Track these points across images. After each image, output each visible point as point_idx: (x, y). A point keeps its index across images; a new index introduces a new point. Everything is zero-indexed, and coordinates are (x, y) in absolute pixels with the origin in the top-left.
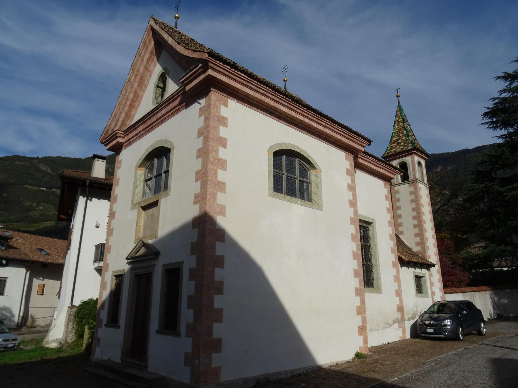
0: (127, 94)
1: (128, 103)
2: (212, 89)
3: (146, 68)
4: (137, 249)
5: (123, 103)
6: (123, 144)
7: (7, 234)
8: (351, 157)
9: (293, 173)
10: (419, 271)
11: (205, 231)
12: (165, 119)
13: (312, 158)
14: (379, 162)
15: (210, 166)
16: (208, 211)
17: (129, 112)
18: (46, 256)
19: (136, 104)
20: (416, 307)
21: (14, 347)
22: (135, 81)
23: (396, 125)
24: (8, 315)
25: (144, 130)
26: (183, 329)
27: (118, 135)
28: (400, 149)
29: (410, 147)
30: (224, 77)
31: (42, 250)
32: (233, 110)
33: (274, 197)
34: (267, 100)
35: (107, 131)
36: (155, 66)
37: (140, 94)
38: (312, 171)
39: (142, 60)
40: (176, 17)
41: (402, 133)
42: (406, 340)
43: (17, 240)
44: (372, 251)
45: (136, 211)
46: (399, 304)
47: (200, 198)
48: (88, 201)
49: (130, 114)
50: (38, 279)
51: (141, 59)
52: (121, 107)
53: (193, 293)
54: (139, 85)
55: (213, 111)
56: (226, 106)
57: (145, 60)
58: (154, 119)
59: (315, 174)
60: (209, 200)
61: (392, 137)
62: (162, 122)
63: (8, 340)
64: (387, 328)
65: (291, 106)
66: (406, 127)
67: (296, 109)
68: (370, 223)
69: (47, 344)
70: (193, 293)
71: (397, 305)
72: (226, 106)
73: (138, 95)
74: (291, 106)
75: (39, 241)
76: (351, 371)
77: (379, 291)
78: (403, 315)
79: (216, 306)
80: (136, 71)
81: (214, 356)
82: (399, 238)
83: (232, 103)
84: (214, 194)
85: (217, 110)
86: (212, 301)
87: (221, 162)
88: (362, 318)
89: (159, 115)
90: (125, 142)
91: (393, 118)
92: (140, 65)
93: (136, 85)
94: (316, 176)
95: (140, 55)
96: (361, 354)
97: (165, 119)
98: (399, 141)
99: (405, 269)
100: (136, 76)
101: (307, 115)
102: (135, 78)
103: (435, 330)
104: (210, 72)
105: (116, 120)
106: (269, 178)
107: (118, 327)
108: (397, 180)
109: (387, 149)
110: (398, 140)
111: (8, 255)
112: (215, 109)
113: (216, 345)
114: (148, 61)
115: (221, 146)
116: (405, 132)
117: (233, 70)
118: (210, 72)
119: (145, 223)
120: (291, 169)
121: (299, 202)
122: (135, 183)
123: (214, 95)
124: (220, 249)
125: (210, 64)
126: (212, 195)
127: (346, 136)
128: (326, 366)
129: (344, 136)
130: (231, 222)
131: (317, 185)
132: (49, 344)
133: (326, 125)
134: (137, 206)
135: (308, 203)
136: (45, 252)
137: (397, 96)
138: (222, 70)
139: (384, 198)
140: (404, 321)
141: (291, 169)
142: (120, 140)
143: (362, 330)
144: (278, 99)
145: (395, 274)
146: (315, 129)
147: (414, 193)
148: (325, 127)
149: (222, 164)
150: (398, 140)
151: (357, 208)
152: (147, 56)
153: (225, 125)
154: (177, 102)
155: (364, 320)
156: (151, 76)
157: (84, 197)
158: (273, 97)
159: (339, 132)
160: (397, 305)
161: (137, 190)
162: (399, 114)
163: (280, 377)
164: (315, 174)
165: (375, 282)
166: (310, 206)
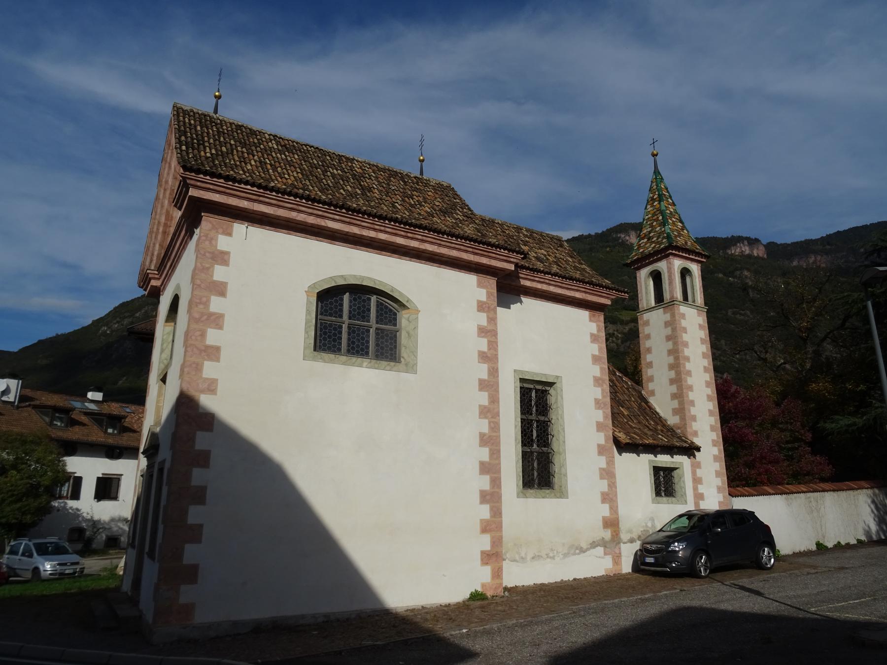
0: (158, 217)
1: (161, 229)
5: (155, 230)
7: (128, 410)
10: (664, 460)
20: (652, 520)
21: (75, 573)
22: (164, 197)
27: (150, 276)
28: (650, 248)
29: (665, 243)
30: (218, 195)
32: (243, 242)
33: (314, 359)
38: (404, 312)
40: (216, 97)
41: (657, 220)
44: (554, 429)
51: (167, 165)
60: (188, 373)
63: (65, 564)
64: (575, 554)
65: (348, 220)
66: (663, 208)
67: (358, 223)
68: (551, 384)
71: (604, 518)
74: (348, 220)
76: (418, 619)
77: (563, 494)
80: (163, 183)
81: (183, 588)
82: (647, 402)
83: (239, 228)
84: (197, 364)
85: (210, 243)
91: (646, 195)
92: (168, 174)
98: (652, 234)
99: (629, 457)
100: (165, 190)
101: (383, 228)
102: (164, 193)
103: (656, 558)
105: (150, 254)
106: (306, 332)
108: (648, 301)
111: (120, 442)
112: (207, 243)
115: (216, 295)
116: (661, 218)
120: (359, 312)
121: (365, 364)
123: (208, 222)
124: (202, 440)
125: (188, 181)
126: (194, 366)
129: (466, 251)
131: (408, 333)
133: (424, 238)
137: (654, 155)
138: (211, 187)
140: (619, 543)
141: (359, 312)
142: (154, 283)
143: (492, 557)
144: (320, 213)
147: (671, 325)
155: (497, 542)
158: (310, 211)
159: (453, 245)
160: (604, 518)
164: (406, 316)
166: (388, 368)
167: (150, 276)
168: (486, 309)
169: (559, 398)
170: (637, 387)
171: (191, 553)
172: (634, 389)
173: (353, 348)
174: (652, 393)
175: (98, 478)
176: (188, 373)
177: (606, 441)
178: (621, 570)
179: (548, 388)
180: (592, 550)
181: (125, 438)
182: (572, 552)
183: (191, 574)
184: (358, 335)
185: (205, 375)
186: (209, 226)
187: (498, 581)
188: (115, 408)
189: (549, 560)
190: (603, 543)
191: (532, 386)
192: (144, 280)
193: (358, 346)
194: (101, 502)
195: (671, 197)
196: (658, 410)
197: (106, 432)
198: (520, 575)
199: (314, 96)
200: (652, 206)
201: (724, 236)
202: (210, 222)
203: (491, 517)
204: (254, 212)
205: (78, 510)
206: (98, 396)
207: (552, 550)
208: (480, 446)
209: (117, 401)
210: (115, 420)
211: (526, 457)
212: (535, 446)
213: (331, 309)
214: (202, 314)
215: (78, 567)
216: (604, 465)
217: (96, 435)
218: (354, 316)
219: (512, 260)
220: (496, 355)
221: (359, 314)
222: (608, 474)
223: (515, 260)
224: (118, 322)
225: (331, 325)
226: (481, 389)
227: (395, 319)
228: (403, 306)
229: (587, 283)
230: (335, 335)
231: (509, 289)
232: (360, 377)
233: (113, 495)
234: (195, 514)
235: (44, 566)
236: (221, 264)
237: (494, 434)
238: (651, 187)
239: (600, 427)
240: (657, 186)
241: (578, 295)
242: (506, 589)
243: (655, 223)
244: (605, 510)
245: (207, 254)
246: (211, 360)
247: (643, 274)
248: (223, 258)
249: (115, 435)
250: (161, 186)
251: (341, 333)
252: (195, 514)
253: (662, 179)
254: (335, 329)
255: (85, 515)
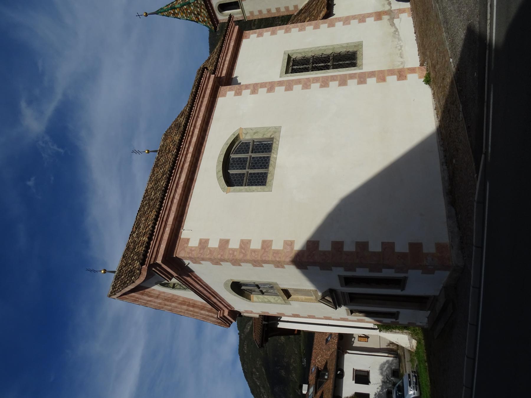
0: (183, 311)
1: (191, 309)
2: (174, 256)
3: (157, 297)
4: (327, 303)
5: (192, 313)
6: (230, 310)
7: (313, 369)
8: (222, 89)
9: (245, 160)
11: (308, 259)
12: (204, 285)
13: (228, 140)
14: (223, 49)
15: (248, 257)
16: (290, 259)
17: (199, 308)
18: (332, 337)
19: (191, 302)
21: (415, 376)
22: (170, 306)
23: (179, 17)
24: (387, 366)
25: (215, 298)
26: (402, 275)
27: (221, 316)
28: (204, 12)
30: (162, 246)
31: (327, 340)
32: (192, 232)
33: (271, 185)
34: (177, 197)
35: (219, 323)
36: (154, 290)
37: (182, 299)
38: (241, 138)
39: (150, 301)
40: (105, 273)
41: (186, 9)
42: (412, 9)
43: (318, 361)
44: (318, 53)
45: (291, 302)
46: (373, 19)
47: (279, 264)
48: (281, 319)
49: (201, 306)
50: (353, 342)
52: (195, 314)
53: (368, 269)
54: (174, 302)
55: (195, 254)
56: (188, 240)
57: (149, 299)
58: (205, 292)
59: (244, 135)
60: (280, 258)
61: (192, 21)
62: (207, 286)
63: (410, 382)
64: (399, 35)
65: (180, 170)
66: (179, 6)
67: (182, 163)
68: (289, 57)
69: (413, 348)
70: (368, 269)
71: (375, 20)
72: (188, 240)
73: (183, 301)
74: (180, 170)
75: (319, 342)
76: (443, 102)
77: (360, 45)
78: (386, 13)
79: (379, 249)
80: (161, 306)
81: (425, 251)
82: (302, 10)
83: (184, 234)
84: (274, 253)
85: (193, 250)
86: (374, 254)
87: (243, 246)
88: (388, 75)
89: (201, 289)
90: (228, 309)
91: (171, 19)
92: (155, 302)
93: (173, 304)
94: (246, 134)
95: (146, 303)
96: (426, 77)
97: (204, 285)
98: (196, 13)
99: (335, 10)
100: (165, 305)
101: (186, 149)
102: (168, 305)
104: (159, 261)
105: (207, 317)
106: (253, 191)
107: (398, 313)
108: (238, 13)
109: (205, 26)
110: (195, 14)
111: (333, 370)
112: (193, 253)
113: (416, 247)
114: (151, 296)
115: (228, 245)
116: (185, 7)
117: (153, 237)
118: (159, 261)
119: (302, 295)
120: (241, 164)
121: (275, 156)
122: (265, 302)
123: (180, 253)
124: (325, 246)
126: (275, 255)
127: (201, 99)
128: (438, 123)
129: (202, 102)
130: (299, 235)
131: (255, 133)
132: (413, 346)
133: (193, 125)
134: (287, 301)
135: (274, 140)
136: (328, 337)
137: (147, 15)
138: (156, 249)
139: (260, 38)
140: (391, 11)
141: (241, 164)
142: (226, 314)
143: (401, 74)
144: (175, 185)
145: (342, 23)
146: (198, 138)
148: (195, 126)
149: (245, 244)
150: (195, 14)
151: (274, 82)
152: (146, 297)
153: (207, 241)
154: (189, 279)
155: (391, 72)
156: (164, 293)
157: (278, 324)
158: (173, 191)
159: (198, 109)
160: (375, 20)
161: (272, 300)
162: (166, 13)
163: (447, 178)
164: (244, 135)
165: (351, 50)
166: (277, 143)
167: (221, 316)
168: (240, 91)
169: (298, 51)
170: (292, 18)
171: (401, 247)
172: (293, 20)
173: (265, 166)
174: (296, 7)
175: (356, 383)
176: (280, 258)
177: (326, 23)
178: (408, 8)
179: (292, 59)
180: (396, 25)
181: (331, 368)
182: (397, 36)
183: (416, 247)
184: (256, 163)
185: (281, 248)
186: (183, 252)
187: (417, 70)
188: (312, 377)
189: (403, 49)
190: (391, 20)
191: (291, 68)
192: (225, 322)
193: (263, 163)
194: (371, 381)
195: (172, 3)
196: (306, 2)
197: (327, 379)
198: (412, 56)
199: (112, 234)
200: (178, 14)
201: (208, 33)
202: (180, 251)
203: (375, 77)
204: (174, 224)
205: (375, 395)
206: (305, 387)
207: (396, 47)
208: (328, 87)
209: (308, 376)
210: (320, 374)
211: (335, 67)
212: (329, 64)
213: (239, 180)
214: (241, 252)
215: (411, 374)
216: (341, 23)
217: (329, 385)
218: (243, 167)
219: (208, 76)
220: (269, 83)
221: (242, 164)
222: (347, 20)
223: (208, 74)
224: (263, 395)
225: (249, 180)
226: (292, 89)
227: (246, 143)
228: (237, 138)
229: (224, 38)
230: (256, 177)
231: (229, 80)
232: (282, 159)
233: (366, 374)
234: (375, 247)
235: (411, 395)
236: (208, 244)
237: (321, 80)
238: (167, 16)
239: (316, 27)
240: (165, 11)
241: (232, 44)
242: (422, 65)
243: (189, 11)
244: (370, 21)
245: (201, 252)
246: (271, 245)
247: (222, 17)
248: (204, 243)
249: (328, 374)
250: (163, 308)
251: (254, 174)
252: (375, 247)
253: (161, 9)
254: (252, 177)
255: (379, 390)
